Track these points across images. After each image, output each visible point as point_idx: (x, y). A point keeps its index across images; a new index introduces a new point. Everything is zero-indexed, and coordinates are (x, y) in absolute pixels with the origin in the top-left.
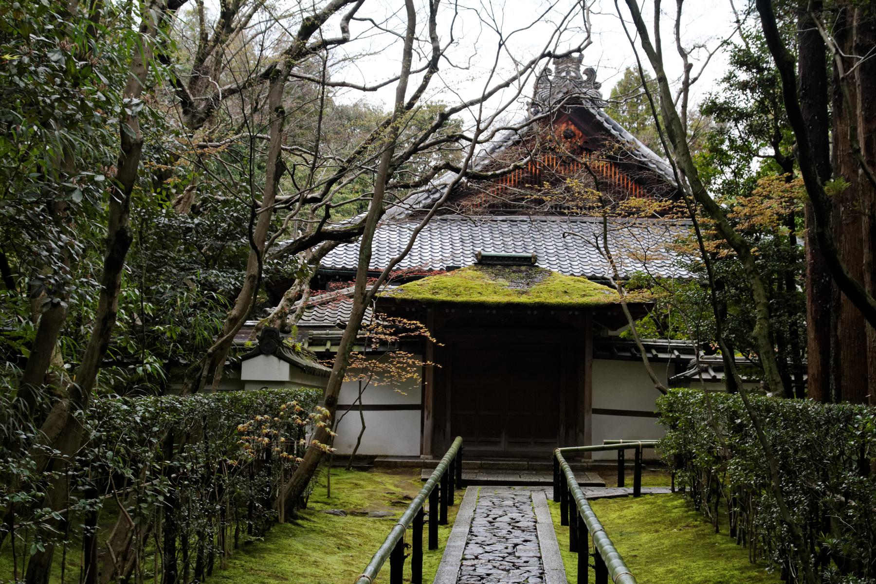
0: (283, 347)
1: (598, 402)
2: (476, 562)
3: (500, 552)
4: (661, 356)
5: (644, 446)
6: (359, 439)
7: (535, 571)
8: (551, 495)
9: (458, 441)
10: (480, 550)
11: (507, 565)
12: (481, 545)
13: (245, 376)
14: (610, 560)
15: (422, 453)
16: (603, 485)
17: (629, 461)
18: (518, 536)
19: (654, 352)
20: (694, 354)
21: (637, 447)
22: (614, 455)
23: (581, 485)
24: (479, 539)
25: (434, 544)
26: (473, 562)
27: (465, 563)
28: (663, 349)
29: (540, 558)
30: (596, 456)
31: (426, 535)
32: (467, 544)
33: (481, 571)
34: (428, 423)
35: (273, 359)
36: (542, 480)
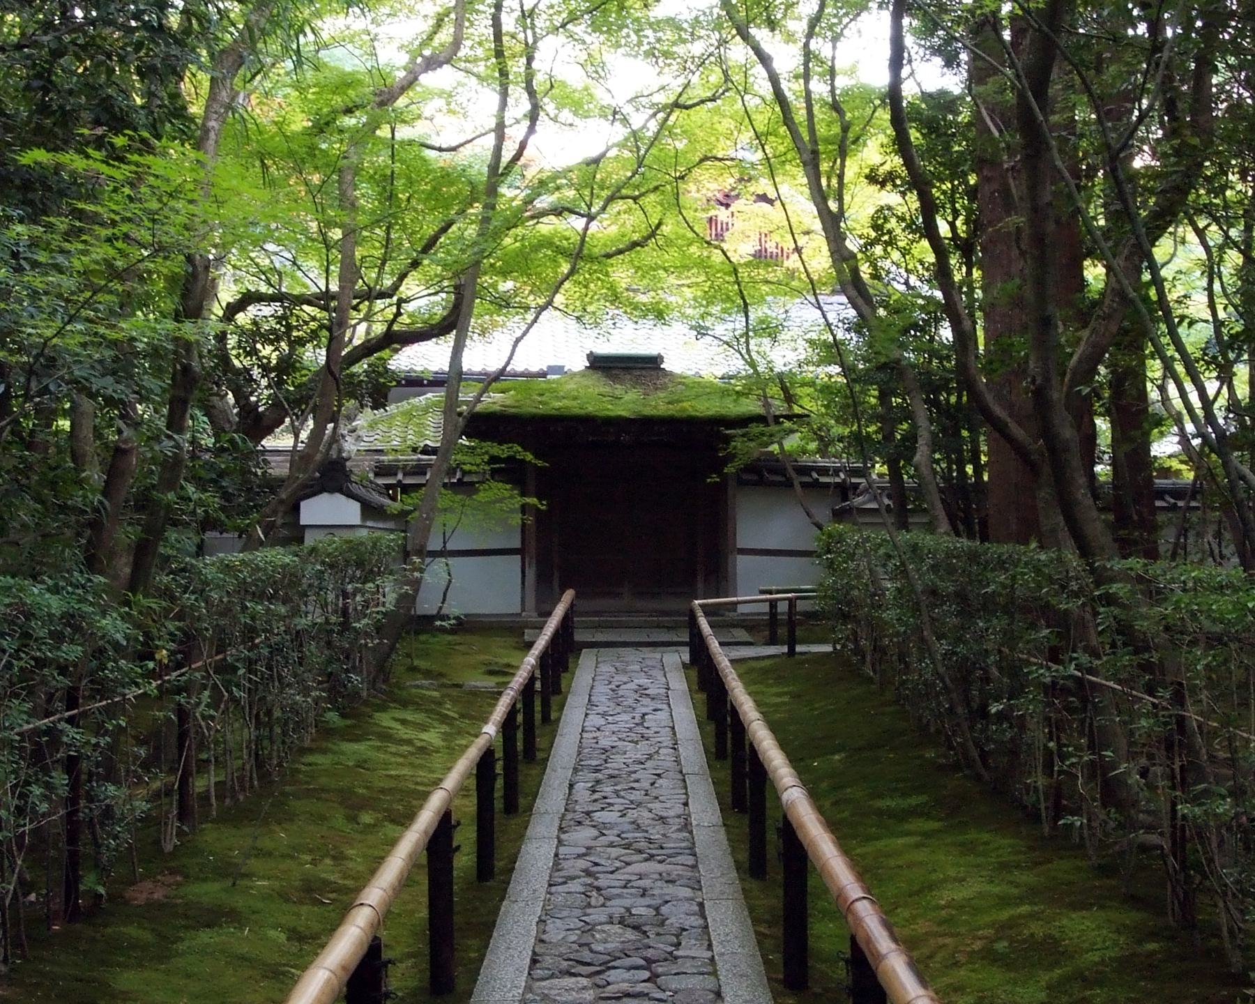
0: (351, 482)
1: (741, 544)
2: (598, 734)
3: (626, 722)
4: (823, 480)
5: (798, 598)
6: (445, 595)
7: (668, 742)
8: (686, 657)
9: (569, 595)
10: (602, 721)
11: (634, 737)
12: (604, 715)
13: (305, 519)
14: (726, 677)
15: (523, 610)
16: (750, 644)
17: (783, 614)
18: (647, 705)
19: (815, 475)
20: (863, 476)
21: (789, 599)
22: (766, 608)
23: (721, 644)
24: (601, 709)
25: (546, 718)
26: (595, 735)
27: (585, 735)
28: (824, 471)
29: (673, 728)
30: (742, 609)
31: (538, 707)
32: (587, 715)
33: (605, 743)
34: (531, 574)
35: (339, 498)
36: (676, 639)
